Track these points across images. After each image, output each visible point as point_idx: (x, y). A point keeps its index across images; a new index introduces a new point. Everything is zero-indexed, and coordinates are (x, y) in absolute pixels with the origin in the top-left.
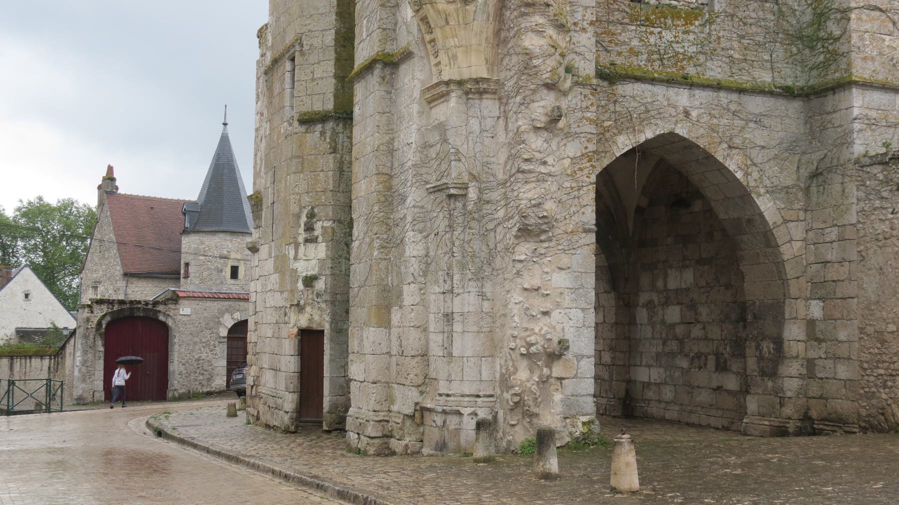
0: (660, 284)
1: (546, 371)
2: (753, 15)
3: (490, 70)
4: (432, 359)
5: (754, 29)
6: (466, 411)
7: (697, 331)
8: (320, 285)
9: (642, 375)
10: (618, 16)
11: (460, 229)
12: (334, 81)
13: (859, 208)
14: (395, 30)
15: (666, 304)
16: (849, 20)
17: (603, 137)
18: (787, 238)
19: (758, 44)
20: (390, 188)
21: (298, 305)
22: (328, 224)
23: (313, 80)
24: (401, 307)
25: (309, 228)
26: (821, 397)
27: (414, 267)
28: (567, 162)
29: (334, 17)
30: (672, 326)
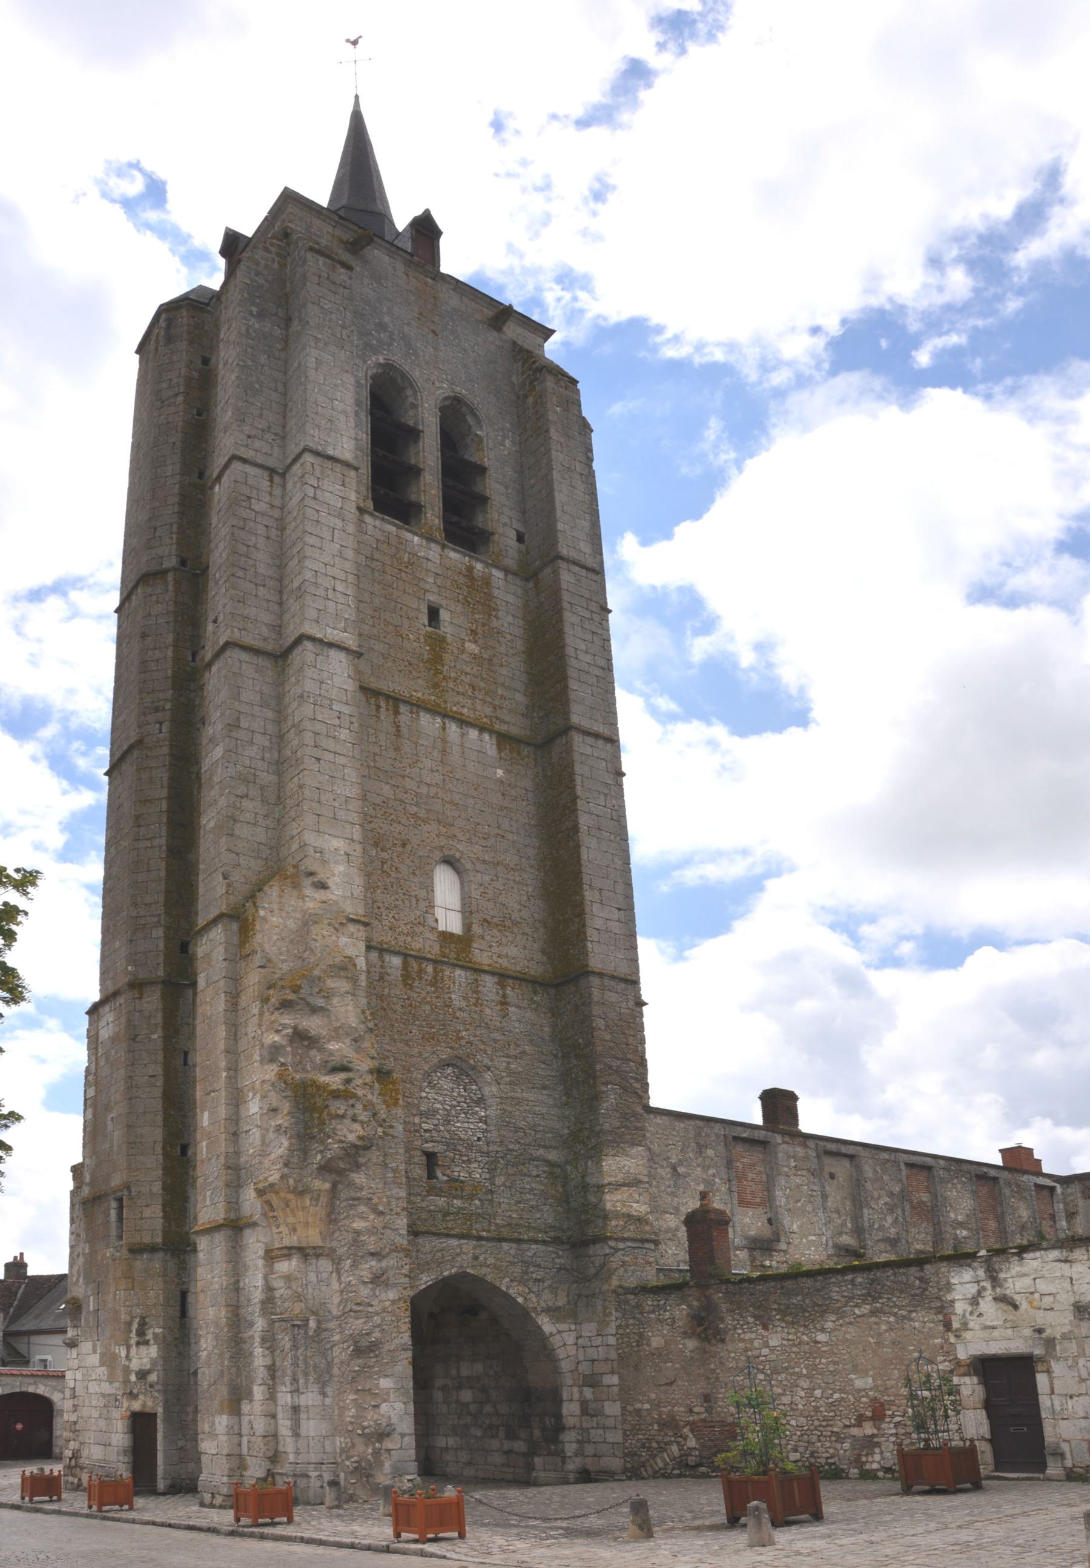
0: (454, 1372)
1: (377, 1445)
2: (528, 1187)
3: (323, 1239)
4: (280, 1438)
5: (528, 1196)
6: (313, 1474)
7: (488, 1408)
8: (153, 1377)
9: (441, 1442)
10: (417, 1190)
11: (303, 1348)
12: (161, 1220)
13: (617, 1323)
14: (237, 1203)
15: (460, 1387)
16: (603, 1193)
17: (412, 1276)
18: (561, 1344)
19: (532, 1207)
20: (237, 1315)
21: (131, 1393)
22: (158, 1331)
23: (142, 1219)
24: (251, 1401)
25: (141, 1333)
26: (595, 1456)
27: (261, 1373)
28: (388, 1303)
29: (160, 1172)
30: (467, 1404)
